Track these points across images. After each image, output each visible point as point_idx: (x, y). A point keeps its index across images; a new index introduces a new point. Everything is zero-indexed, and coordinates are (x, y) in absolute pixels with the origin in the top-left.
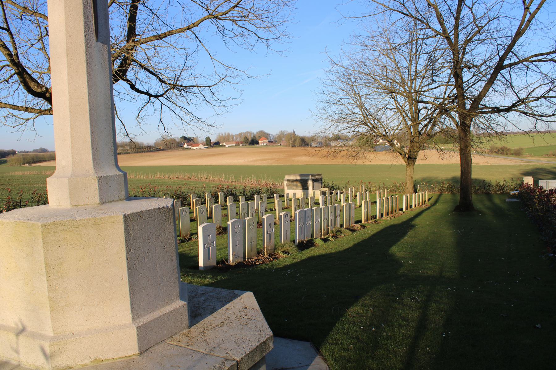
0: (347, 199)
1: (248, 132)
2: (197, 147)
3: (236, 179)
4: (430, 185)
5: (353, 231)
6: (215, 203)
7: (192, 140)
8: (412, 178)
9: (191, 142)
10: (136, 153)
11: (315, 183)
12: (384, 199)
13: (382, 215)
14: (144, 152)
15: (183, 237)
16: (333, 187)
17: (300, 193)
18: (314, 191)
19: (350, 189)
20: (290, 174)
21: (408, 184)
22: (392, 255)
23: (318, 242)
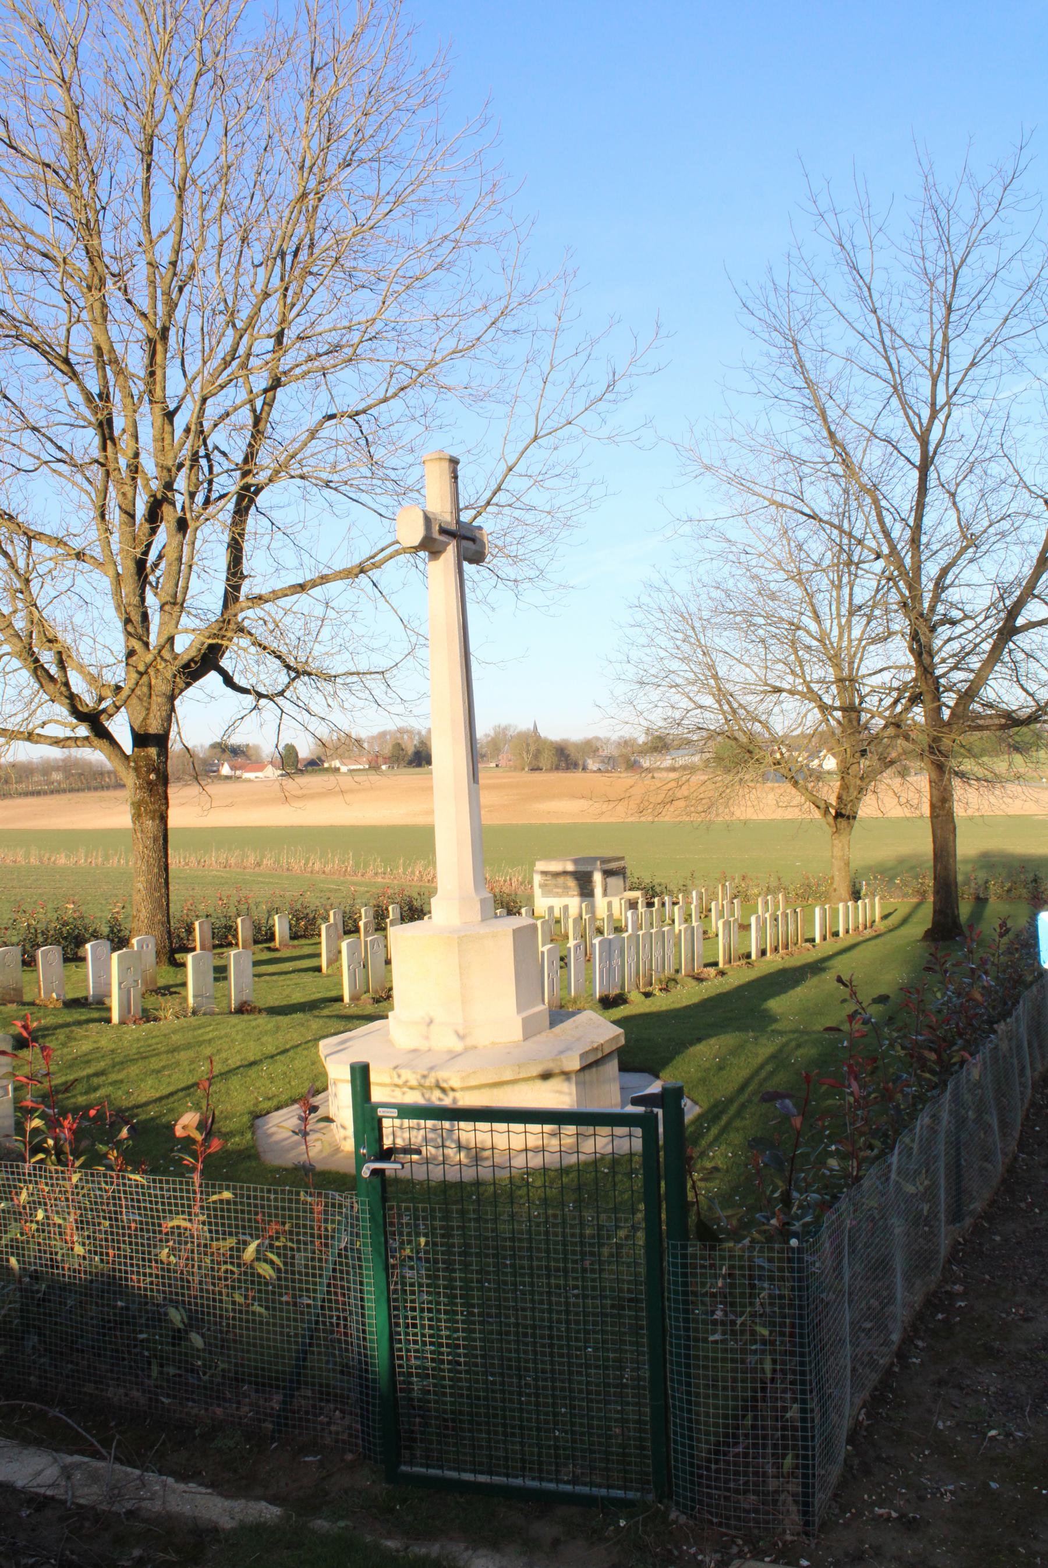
0: (688, 918)
1: (401, 731)
2: (260, 774)
3: (385, 867)
4: (891, 879)
5: (699, 979)
6: (377, 930)
7: (243, 752)
8: (847, 864)
9: (240, 760)
10: (83, 790)
11: (609, 880)
12: (767, 915)
13: (763, 953)
14: (108, 788)
15: (376, 992)
16: (652, 888)
17: (574, 903)
18: (607, 899)
19: (694, 893)
20: (548, 857)
21: (837, 879)
22: (766, 1010)
23: (634, 996)
